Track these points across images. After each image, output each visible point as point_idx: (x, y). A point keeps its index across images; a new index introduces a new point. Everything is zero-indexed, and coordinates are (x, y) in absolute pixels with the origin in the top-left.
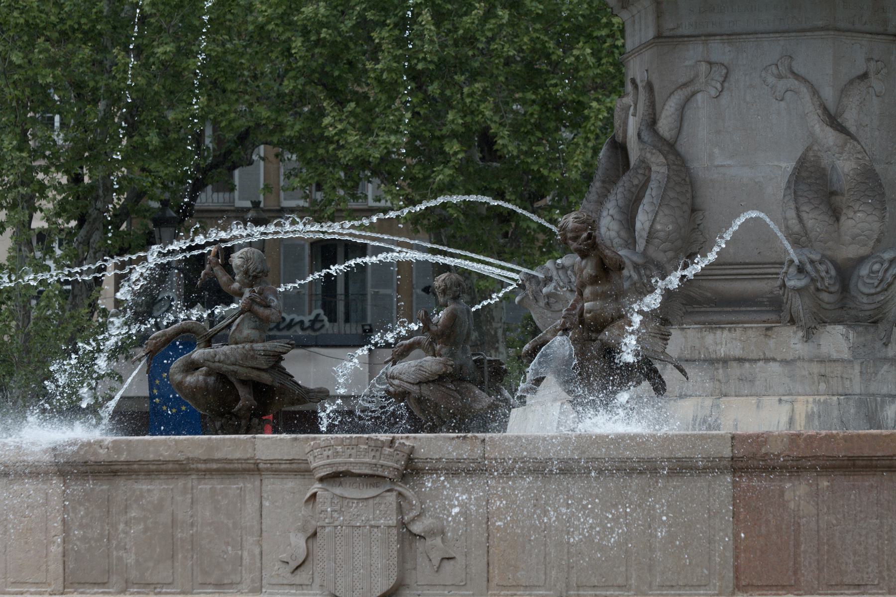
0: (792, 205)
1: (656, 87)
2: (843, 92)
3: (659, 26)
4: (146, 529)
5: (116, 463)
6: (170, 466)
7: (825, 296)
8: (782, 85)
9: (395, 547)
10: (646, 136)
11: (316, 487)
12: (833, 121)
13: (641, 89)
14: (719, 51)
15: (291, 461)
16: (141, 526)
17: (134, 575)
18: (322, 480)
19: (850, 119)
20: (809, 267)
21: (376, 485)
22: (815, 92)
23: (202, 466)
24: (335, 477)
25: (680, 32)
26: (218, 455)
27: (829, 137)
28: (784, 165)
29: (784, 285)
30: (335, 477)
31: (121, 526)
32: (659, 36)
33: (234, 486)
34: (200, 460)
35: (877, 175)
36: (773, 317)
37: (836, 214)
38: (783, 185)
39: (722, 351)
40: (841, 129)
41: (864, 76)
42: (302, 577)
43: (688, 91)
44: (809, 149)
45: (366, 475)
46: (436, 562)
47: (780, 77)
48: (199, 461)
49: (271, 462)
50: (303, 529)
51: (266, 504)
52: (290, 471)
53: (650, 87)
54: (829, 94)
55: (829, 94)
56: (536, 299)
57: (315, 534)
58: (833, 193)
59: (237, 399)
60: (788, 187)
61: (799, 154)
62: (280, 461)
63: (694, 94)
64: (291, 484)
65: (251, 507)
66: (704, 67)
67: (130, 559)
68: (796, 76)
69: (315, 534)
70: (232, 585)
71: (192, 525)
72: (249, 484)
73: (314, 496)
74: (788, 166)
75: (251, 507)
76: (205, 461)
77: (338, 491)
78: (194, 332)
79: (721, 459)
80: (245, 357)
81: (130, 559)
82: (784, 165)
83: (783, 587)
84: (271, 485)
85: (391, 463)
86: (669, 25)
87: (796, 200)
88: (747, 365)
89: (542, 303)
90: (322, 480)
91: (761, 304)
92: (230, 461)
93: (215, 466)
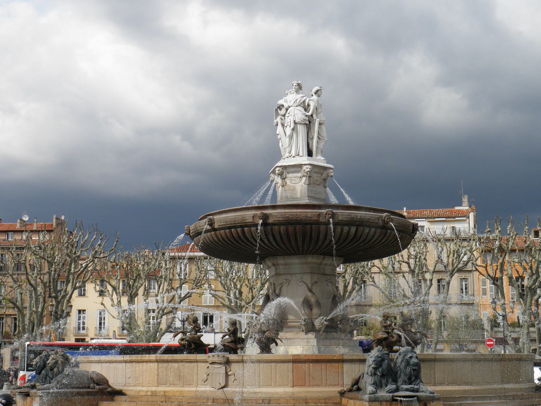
0: (303, 308)
1: (275, 284)
2: (312, 285)
3: (276, 272)
4: (174, 373)
5: (169, 360)
6: (179, 361)
7: (309, 326)
8: (300, 284)
9: (224, 377)
10: (273, 294)
11: (208, 365)
12: (310, 291)
13: (272, 284)
14: (289, 277)
15: (204, 360)
16: (173, 373)
17: (172, 382)
18: (210, 364)
19: (314, 290)
20: (306, 320)
21: (221, 365)
22: (307, 285)
23: (186, 361)
24: (213, 363)
25: (281, 273)
26: (189, 359)
27: (309, 294)
28: (301, 300)
29: (301, 324)
30: (213, 363)
31: (169, 373)
32: (276, 274)
33: (192, 364)
34: (484, 361)
35: (319, 302)
36: (299, 330)
37: (311, 309)
38: (301, 304)
39: (288, 337)
40: (312, 293)
41: (316, 282)
42: (206, 383)
43: (281, 285)
44: (306, 296)
45: (219, 363)
46: (233, 381)
47: (300, 282)
48: (185, 360)
49: (200, 360)
50: (206, 373)
51: (199, 368)
52: (430, 361)
53: (274, 284)
54: (310, 286)
55: (310, 286)
56: (251, 326)
57: (208, 375)
58: (311, 305)
59: (192, 346)
60: (302, 304)
61: (304, 298)
62: (202, 360)
63: (283, 286)
64: (204, 364)
65: (196, 369)
66: (285, 280)
67: (171, 379)
68: (303, 282)
69: (208, 375)
70: (192, 385)
71: (184, 373)
72: (195, 364)
73: (208, 367)
74: (302, 300)
75: (196, 369)
76: (187, 360)
77: (213, 366)
78: (383, 360)
79: (290, 360)
80: (193, 337)
81: (171, 379)
82: (301, 300)
83: (303, 385)
84: (200, 364)
85: (222, 360)
86: (278, 272)
87: (303, 307)
88: (294, 340)
89: (252, 327)
90: (210, 364)
91: (296, 327)
92: (192, 360)
93: (188, 360)
